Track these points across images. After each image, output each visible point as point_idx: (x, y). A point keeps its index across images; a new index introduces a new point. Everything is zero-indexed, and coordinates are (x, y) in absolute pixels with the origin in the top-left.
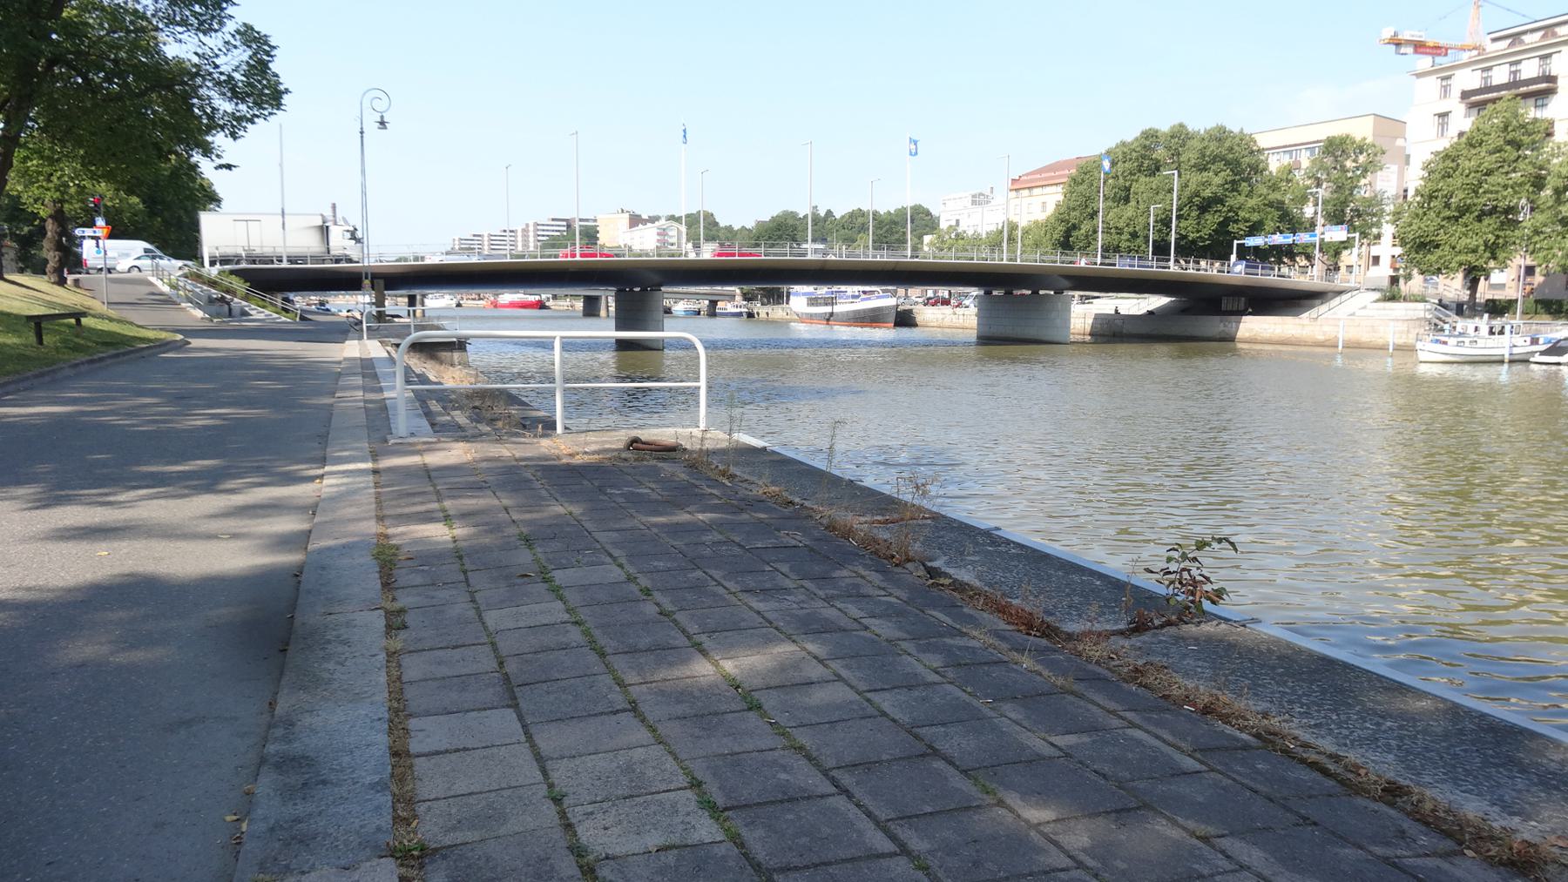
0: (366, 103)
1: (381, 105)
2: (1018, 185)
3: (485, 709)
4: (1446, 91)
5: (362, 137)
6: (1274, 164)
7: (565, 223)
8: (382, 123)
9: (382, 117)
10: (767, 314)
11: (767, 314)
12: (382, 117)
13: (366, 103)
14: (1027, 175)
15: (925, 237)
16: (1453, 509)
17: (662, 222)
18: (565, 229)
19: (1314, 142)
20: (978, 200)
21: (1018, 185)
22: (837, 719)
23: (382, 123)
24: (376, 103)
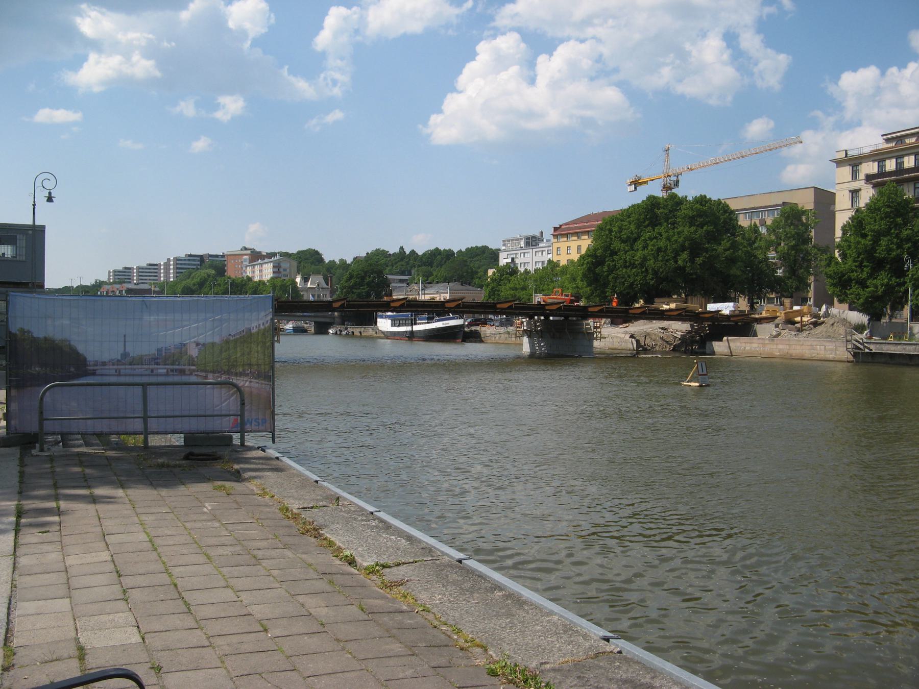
0: (38, 183)
1: (49, 185)
2: (560, 232)
3: (166, 433)
4: (855, 175)
5: (34, 202)
6: (744, 222)
7: (199, 259)
8: (50, 199)
9: (50, 193)
10: (360, 333)
11: (360, 333)
12: (50, 193)
13: (38, 183)
14: (566, 224)
15: (489, 271)
16: (623, 543)
17: (278, 257)
18: (199, 263)
19: (774, 206)
20: (532, 242)
21: (560, 232)
22: (374, 660)
23: (50, 199)
24: (46, 184)
